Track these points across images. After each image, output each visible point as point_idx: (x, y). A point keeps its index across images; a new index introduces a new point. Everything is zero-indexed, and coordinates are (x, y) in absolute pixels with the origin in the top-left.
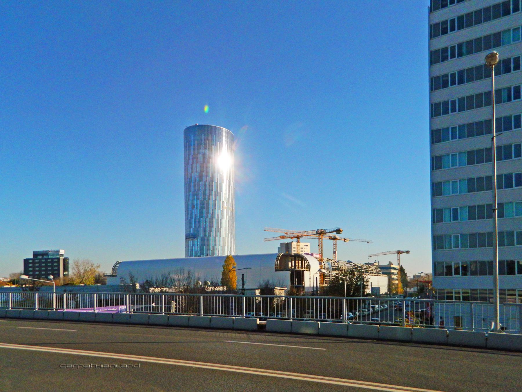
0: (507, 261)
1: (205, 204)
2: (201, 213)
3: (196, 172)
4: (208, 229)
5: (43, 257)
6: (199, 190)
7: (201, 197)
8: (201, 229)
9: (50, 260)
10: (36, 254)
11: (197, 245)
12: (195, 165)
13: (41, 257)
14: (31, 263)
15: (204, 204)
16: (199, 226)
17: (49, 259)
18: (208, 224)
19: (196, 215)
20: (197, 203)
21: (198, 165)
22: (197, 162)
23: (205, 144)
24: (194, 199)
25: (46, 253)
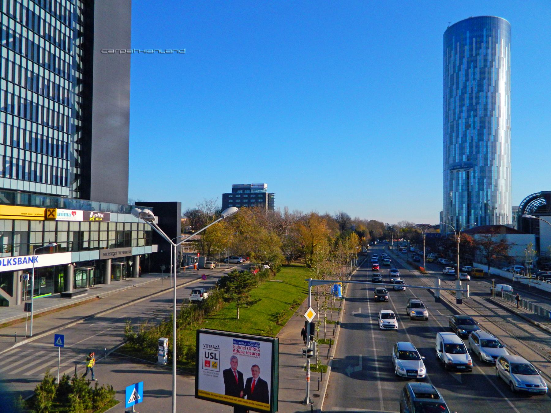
0: (148, 254)
1: (487, 73)
2: (481, 134)
3: (474, 79)
4: (489, 156)
5: (243, 192)
6: (477, 103)
7: (481, 113)
8: (480, 156)
9: (254, 196)
10: (236, 189)
11: (474, 177)
12: (471, 71)
13: (241, 192)
14: (231, 199)
15: (484, 73)
16: (478, 152)
17: (253, 194)
18: (489, 150)
19: (472, 137)
20: (474, 122)
21: (477, 119)
22: (475, 116)
23: (487, 42)
24: (469, 116)
25: (247, 188)
